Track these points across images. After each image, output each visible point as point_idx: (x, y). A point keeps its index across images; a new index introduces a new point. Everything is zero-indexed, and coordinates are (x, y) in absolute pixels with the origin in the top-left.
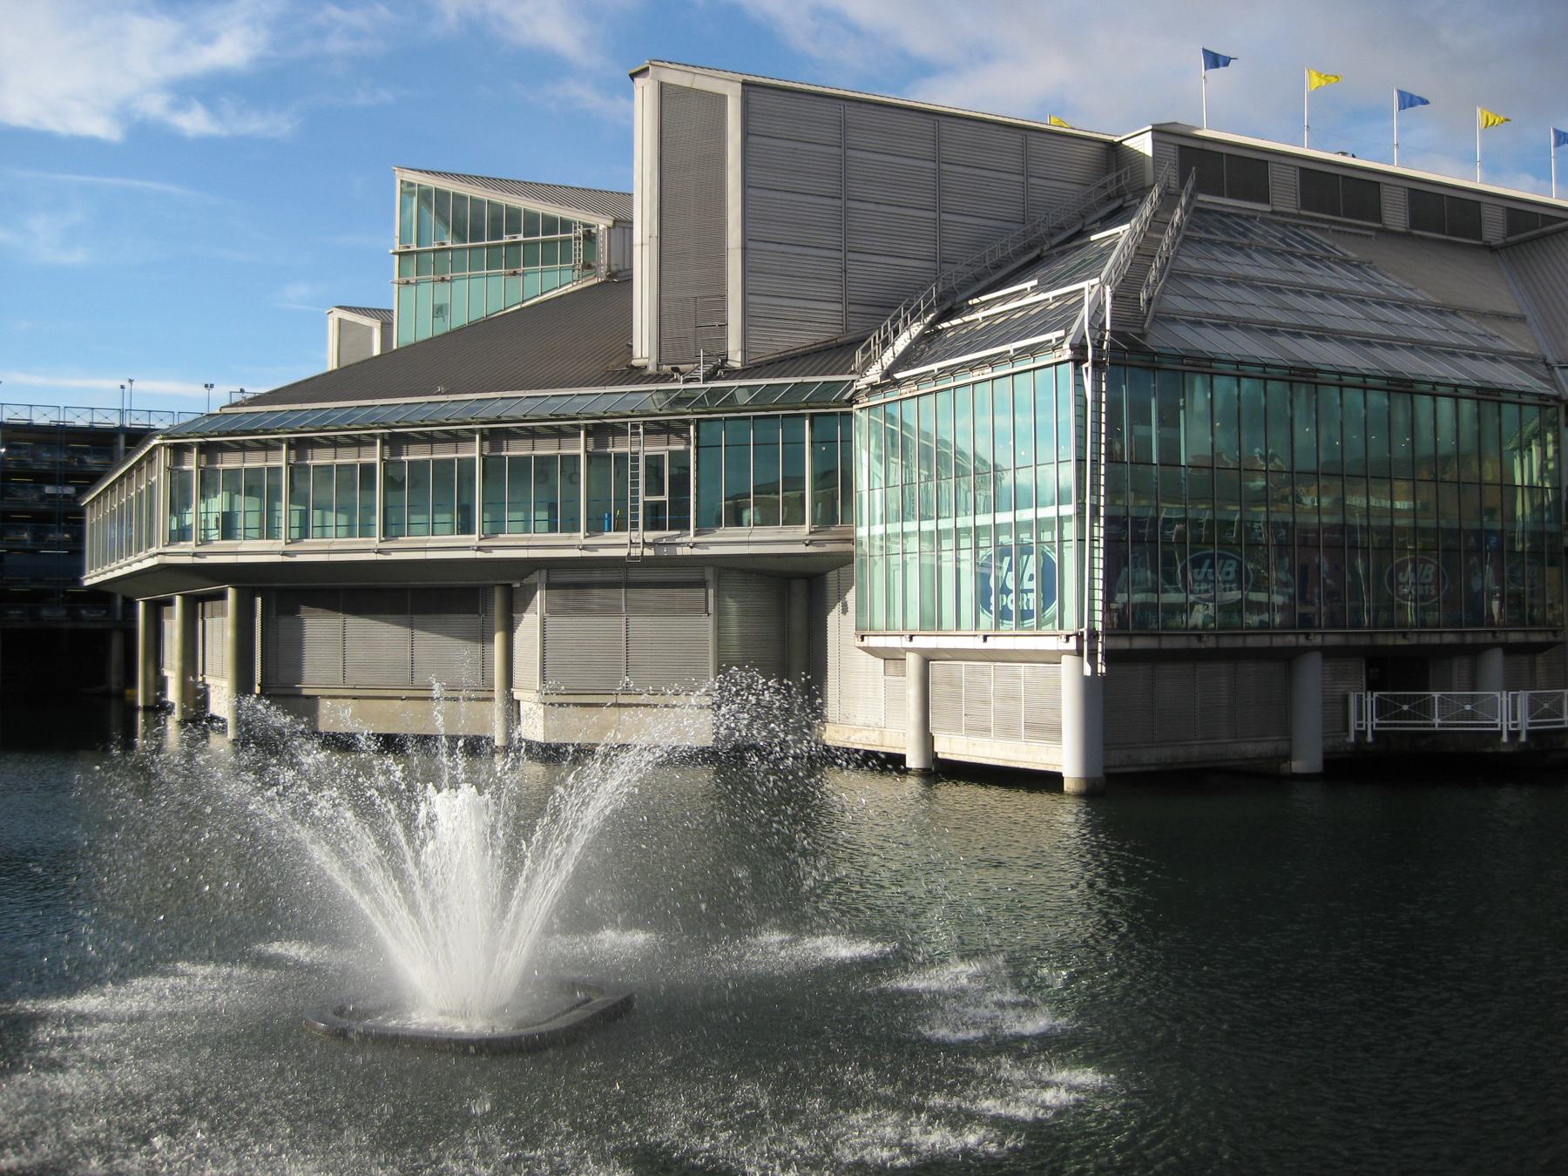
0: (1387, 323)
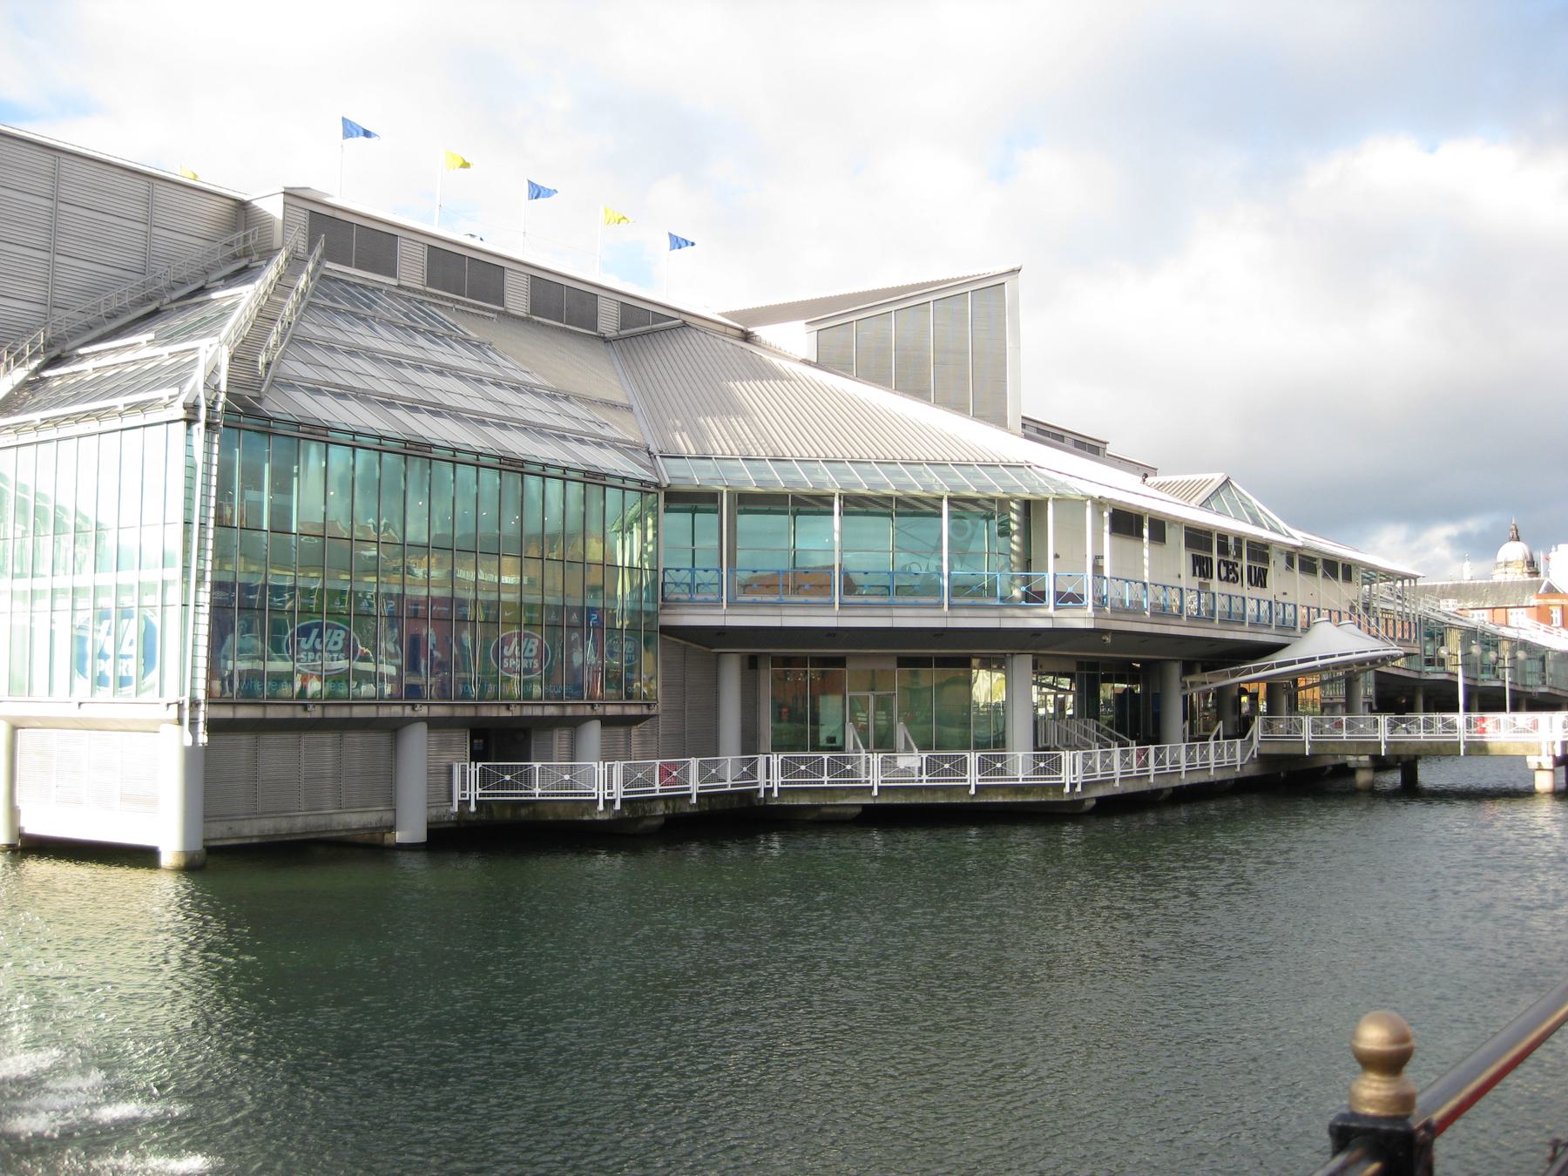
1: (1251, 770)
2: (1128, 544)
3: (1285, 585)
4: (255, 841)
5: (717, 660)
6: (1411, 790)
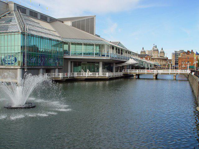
1: (123, 76)
3: (125, 55)
5: (68, 62)
6: (138, 78)
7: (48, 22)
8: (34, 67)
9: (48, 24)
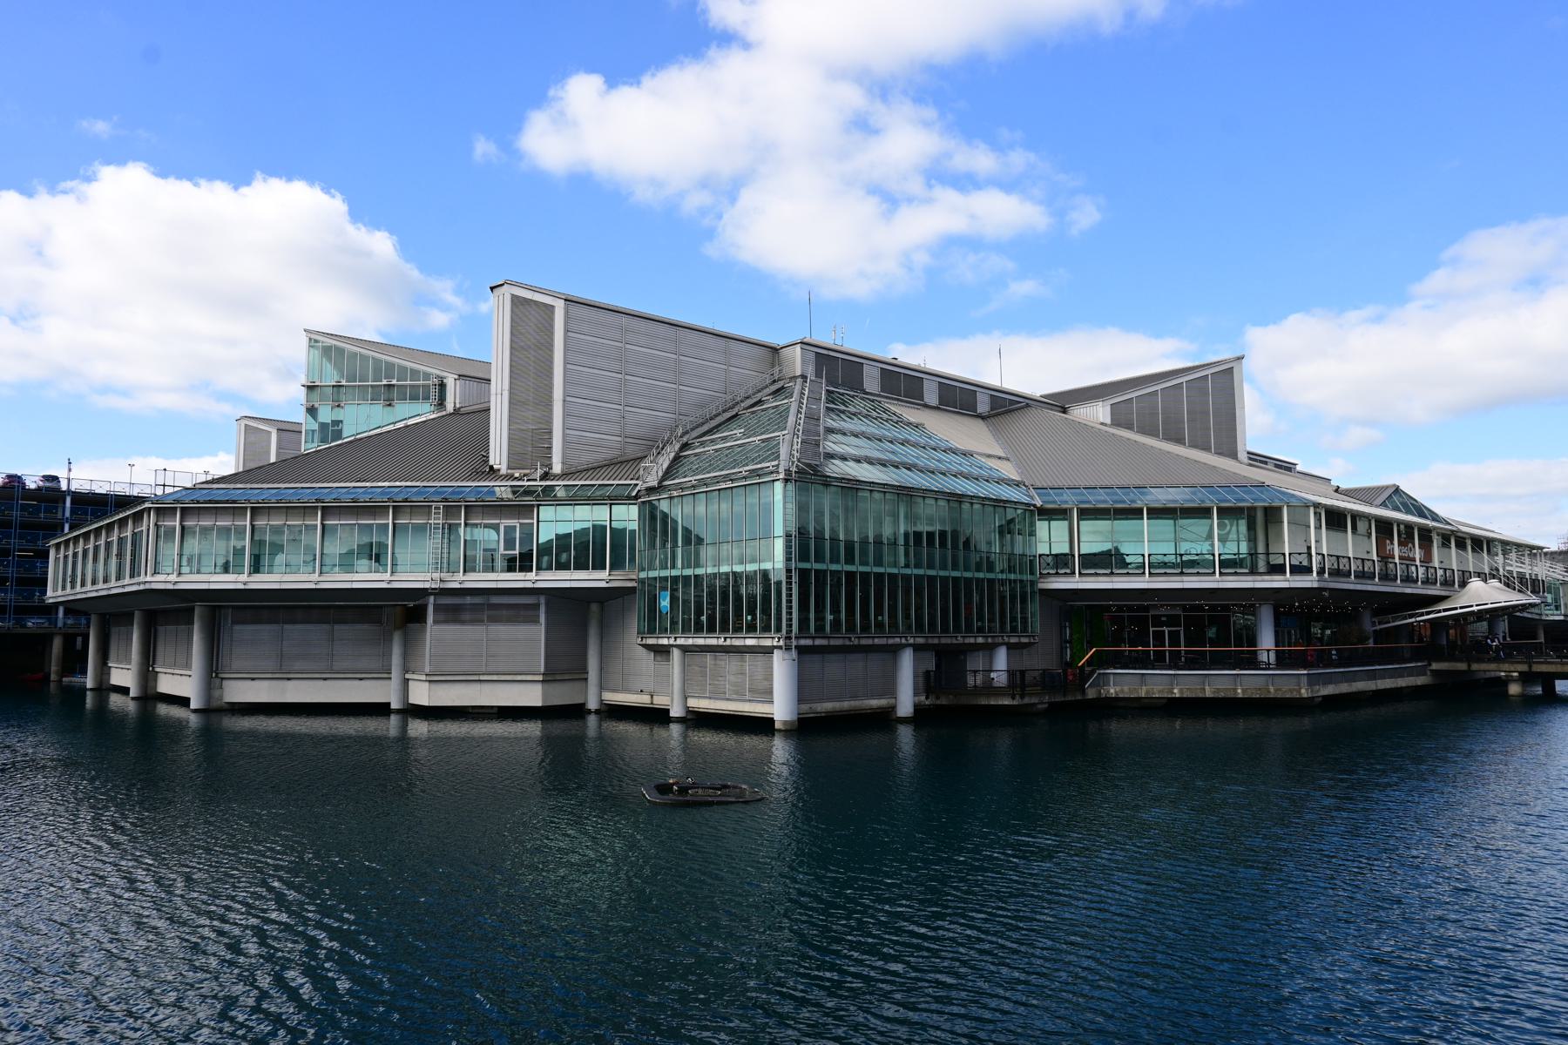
0: (893, 453)
2: (1338, 535)
4: (823, 715)
7: (926, 406)
8: (864, 642)
9: (979, 423)
